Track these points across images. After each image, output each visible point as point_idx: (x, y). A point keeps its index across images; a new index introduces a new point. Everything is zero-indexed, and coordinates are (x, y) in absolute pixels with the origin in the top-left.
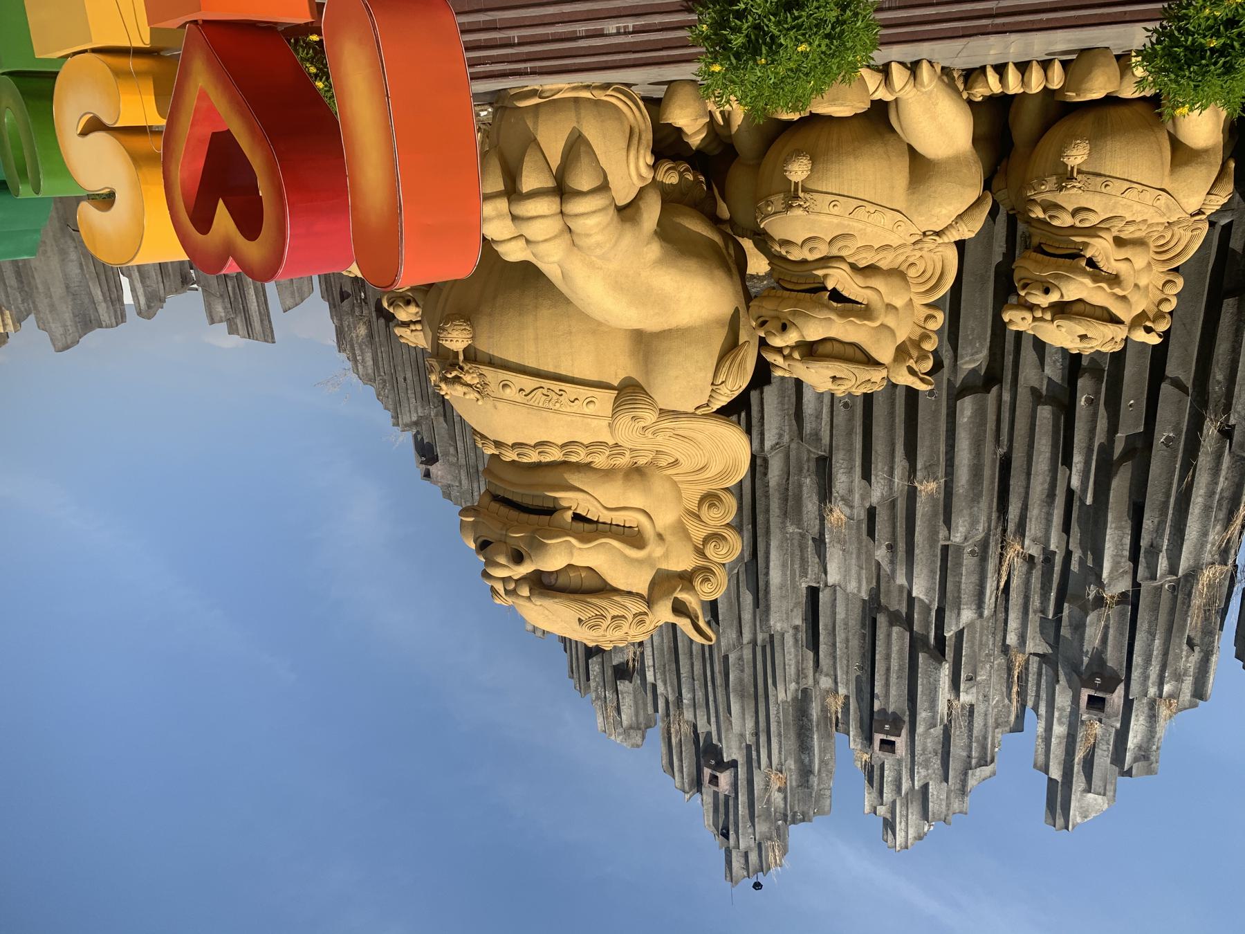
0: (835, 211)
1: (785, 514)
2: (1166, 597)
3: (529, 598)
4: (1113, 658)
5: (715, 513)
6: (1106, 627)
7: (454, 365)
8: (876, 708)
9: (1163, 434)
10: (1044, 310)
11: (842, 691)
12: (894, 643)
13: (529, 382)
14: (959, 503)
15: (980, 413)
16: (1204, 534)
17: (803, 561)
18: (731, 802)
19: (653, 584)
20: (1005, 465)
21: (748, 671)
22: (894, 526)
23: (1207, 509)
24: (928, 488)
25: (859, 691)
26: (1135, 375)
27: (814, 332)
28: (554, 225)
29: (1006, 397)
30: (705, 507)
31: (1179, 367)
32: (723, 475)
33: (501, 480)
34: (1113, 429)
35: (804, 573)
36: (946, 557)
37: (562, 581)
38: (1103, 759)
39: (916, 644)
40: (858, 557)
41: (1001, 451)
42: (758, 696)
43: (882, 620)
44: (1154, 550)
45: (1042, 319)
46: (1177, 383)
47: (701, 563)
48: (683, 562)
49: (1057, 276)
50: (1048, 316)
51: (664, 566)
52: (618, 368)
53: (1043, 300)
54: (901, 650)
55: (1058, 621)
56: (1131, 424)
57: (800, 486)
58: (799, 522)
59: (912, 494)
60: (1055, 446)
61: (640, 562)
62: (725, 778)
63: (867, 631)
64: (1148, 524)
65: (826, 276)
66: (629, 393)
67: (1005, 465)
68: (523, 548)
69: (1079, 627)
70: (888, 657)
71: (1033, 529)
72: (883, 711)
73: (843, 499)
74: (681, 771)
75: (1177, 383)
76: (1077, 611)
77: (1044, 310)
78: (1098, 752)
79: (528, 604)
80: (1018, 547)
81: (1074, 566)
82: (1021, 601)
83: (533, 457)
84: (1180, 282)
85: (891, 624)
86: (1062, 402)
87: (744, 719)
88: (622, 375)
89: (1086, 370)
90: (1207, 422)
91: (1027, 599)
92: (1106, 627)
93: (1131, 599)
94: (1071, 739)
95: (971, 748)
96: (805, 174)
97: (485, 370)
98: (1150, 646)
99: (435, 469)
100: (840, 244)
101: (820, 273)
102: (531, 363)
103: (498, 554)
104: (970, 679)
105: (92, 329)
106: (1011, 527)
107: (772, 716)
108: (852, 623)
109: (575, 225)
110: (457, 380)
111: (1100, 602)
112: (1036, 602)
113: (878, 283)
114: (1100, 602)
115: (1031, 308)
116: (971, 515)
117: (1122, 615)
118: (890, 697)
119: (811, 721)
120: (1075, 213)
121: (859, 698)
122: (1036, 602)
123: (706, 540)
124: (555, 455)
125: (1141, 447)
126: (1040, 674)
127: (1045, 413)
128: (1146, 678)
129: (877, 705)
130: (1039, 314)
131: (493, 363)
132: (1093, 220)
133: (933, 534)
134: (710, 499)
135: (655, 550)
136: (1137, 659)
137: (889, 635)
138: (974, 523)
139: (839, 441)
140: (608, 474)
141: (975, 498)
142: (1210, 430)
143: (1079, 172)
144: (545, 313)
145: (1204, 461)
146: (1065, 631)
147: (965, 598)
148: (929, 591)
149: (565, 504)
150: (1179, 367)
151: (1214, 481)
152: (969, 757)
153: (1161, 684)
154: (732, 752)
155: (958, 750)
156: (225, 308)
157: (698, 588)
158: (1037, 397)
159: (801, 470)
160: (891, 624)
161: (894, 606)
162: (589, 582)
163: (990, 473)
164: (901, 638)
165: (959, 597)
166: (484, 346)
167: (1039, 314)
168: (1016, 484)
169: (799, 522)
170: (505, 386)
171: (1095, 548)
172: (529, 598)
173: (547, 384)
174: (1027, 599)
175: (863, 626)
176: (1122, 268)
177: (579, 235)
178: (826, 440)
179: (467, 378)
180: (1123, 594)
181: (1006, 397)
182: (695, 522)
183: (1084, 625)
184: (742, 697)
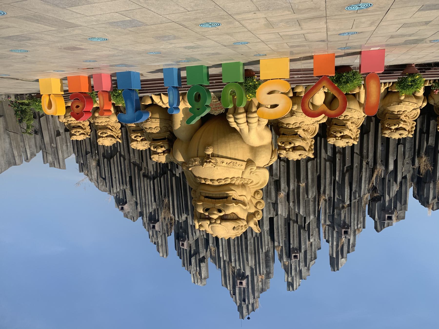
0: (302, 116)
1: (267, 197)
2: (356, 203)
3: (220, 223)
4: (347, 221)
5: (259, 196)
6: (345, 213)
7: (209, 158)
8: (291, 247)
9: (355, 165)
10: (339, 137)
11: (281, 245)
12: (294, 228)
13: (229, 161)
14: (310, 188)
15: (313, 165)
16: (365, 186)
17: (269, 210)
18: (246, 290)
19: (247, 217)
20: (319, 178)
21: (253, 246)
22: (295, 197)
23: (365, 181)
24: (303, 185)
25: (285, 244)
26: (348, 152)
27: (297, 144)
28: (244, 120)
29: (318, 161)
30: (256, 194)
31: (357, 150)
32: (262, 185)
33: (207, 191)
34: (344, 165)
35: (270, 213)
36: (307, 203)
37: (229, 217)
38: (345, 249)
39: (300, 228)
40: (285, 206)
41: (318, 174)
42: (256, 253)
43: (291, 222)
44: (355, 193)
45: (338, 139)
46: (357, 153)
47: (256, 210)
48: (252, 210)
49: (343, 130)
50: (340, 139)
51: (249, 211)
52: (247, 156)
53: (339, 135)
54: (296, 230)
55: (333, 215)
56: (348, 164)
57: (271, 189)
58: (271, 199)
59: (299, 187)
60: (331, 171)
61: (244, 210)
62: (244, 282)
63: (287, 227)
64: (354, 186)
65: (298, 131)
66: (249, 162)
67: (319, 178)
68: (222, 208)
69: (339, 215)
70: (293, 232)
71: (327, 192)
72: (293, 248)
73: (283, 190)
74: (230, 284)
75: (357, 153)
76: (338, 211)
77: (339, 137)
78: (344, 247)
79: (220, 225)
80: (324, 197)
81: (336, 200)
82: (324, 211)
83: (223, 182)
84: (360, 131)
85: (294, 223)
86: (332, 160)
87: (252, 261)
88: (247, 159)
89: (337, 152)
90: (364, 162)
91: (325, 210)
92: (345, 213)
93: (350, 205)
94: (337, 245)
95: (312, 255)
96: (296, 108)
97: (217, 159)
98: (354, 216)
99: (126, 207)
100: (301, 124)
101: (296, 131)
102: (229, 156)
103: (214, 211)
104: (312, 235)
105: (11, 166)
106: (322, 192)
107: (261, 258)
108: (282, 225)
109: (250, 120)
110: (210, 162)
111: (343, 207)
112: (328, 211)
113: (306, 133)
114: (343, 207)
115: (335, 137)
116: (312, 191)
117: (348, 210)
118: (294, 244)
119: (270, 257)
120: (398, 112)
121: (285, 246)
122: (328, 211)
123: (257, 204)
124: (228, 181)
125: (351, 168)
126: (329, 230)
127: (328, 163)
128: (354, 224)
129: (291, 247)
130: (337, 138)
131: (218, 156)
132: (348, 118)
133: (304, 196)
134: (257, 192)
135: (248, 207)
136: (352, 220)
137: (293, 226)
138: (313, 193)
139: (282, 175)
140: (238, 186)
141: (313, 187)
142: (364, 163)
143: (296, 112)
144: (238, 142)
145: (364, 170)
146: (336, 217)
147: (311, 213)
148: (303, 212)
149: (230, 195)
150: (357, 150)
151: (366, 174)
152: (312, 258)
153: (358, 225)
154: (248, 273)
155: (309, 257)
156: (52, 158)
157: (257, 217)
158: (326, 160)
159: (271, 184)
160: (294, 223)
161: (293, 219)
162: (235, 217)
163: (316, 180)
164: (296, 226)
165: (310, 213)
166: (216, 153)
167: (337, 138)
168: (322, 182)
169: (271, 199)
170: (223, 162)
171: (342, 194)
172: (220, 223)
173: (235, 161)
174: (325, 210)
175: (285, 225)
176: (406, 120)
177: (250, 123)
178: (278, 176)
179: (213, 161)
180: (348, 205)
181: (318, 161)
182: (254, 199)
183: (341, 214)
184: (251, 254)
